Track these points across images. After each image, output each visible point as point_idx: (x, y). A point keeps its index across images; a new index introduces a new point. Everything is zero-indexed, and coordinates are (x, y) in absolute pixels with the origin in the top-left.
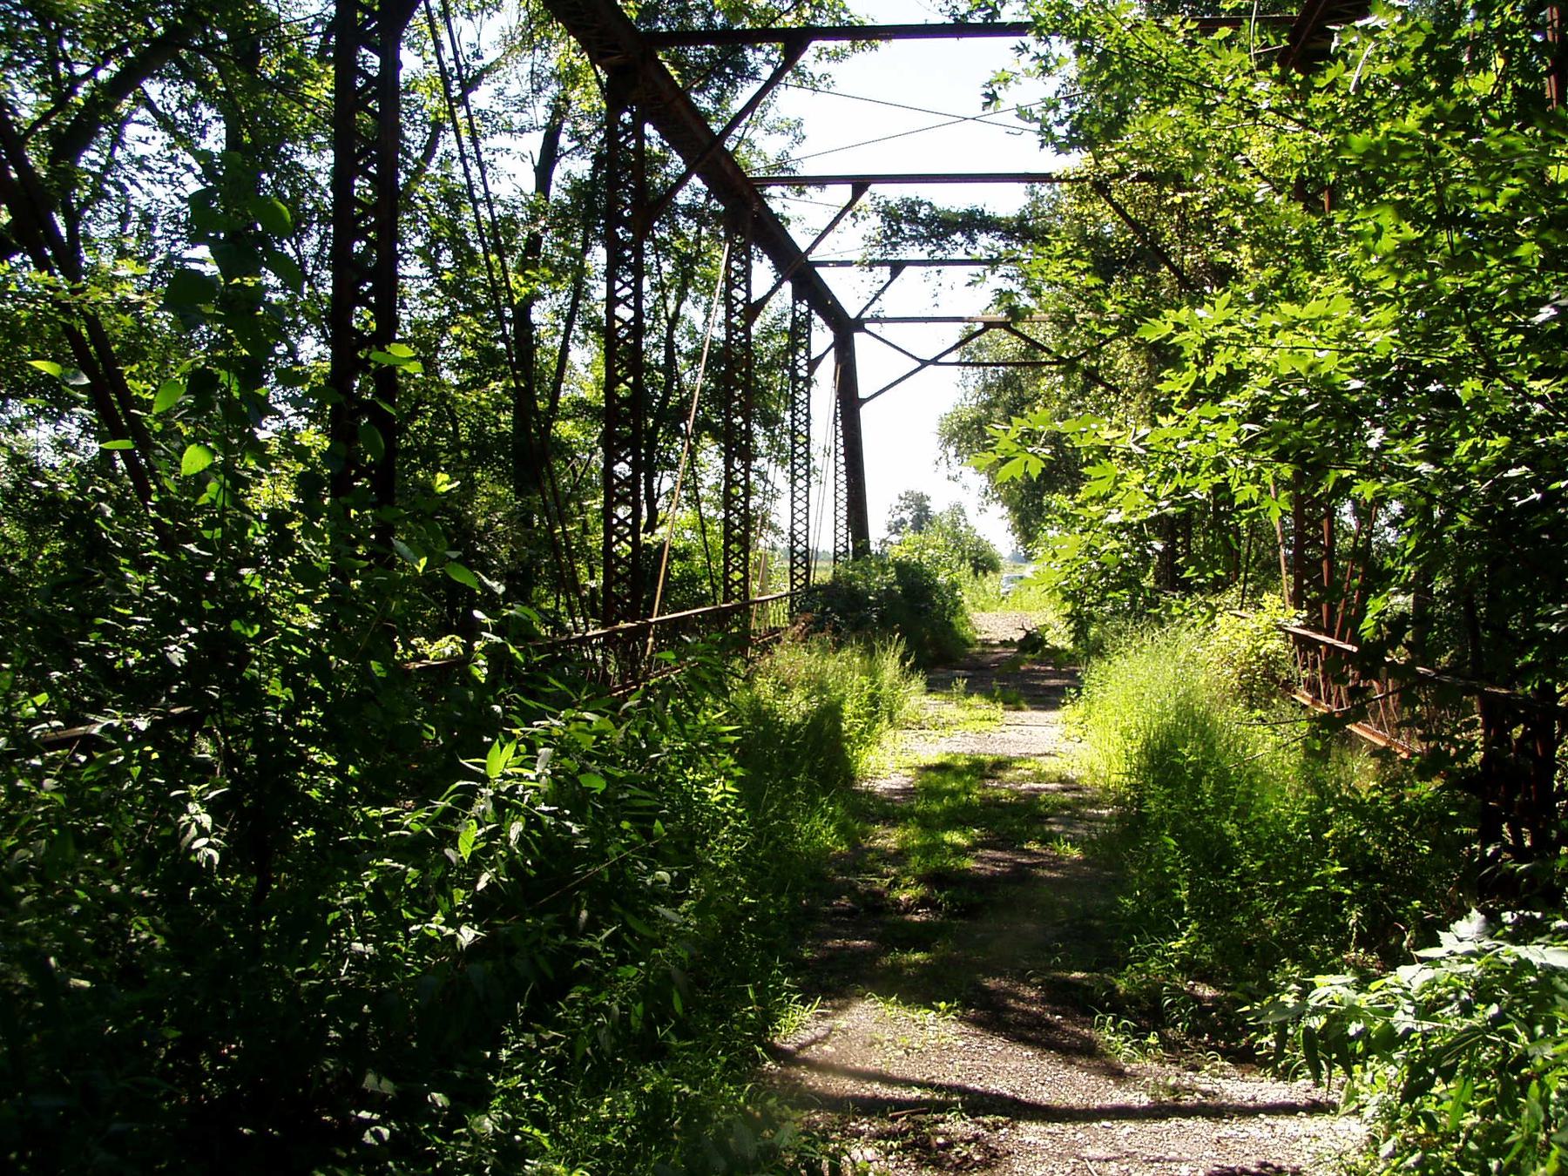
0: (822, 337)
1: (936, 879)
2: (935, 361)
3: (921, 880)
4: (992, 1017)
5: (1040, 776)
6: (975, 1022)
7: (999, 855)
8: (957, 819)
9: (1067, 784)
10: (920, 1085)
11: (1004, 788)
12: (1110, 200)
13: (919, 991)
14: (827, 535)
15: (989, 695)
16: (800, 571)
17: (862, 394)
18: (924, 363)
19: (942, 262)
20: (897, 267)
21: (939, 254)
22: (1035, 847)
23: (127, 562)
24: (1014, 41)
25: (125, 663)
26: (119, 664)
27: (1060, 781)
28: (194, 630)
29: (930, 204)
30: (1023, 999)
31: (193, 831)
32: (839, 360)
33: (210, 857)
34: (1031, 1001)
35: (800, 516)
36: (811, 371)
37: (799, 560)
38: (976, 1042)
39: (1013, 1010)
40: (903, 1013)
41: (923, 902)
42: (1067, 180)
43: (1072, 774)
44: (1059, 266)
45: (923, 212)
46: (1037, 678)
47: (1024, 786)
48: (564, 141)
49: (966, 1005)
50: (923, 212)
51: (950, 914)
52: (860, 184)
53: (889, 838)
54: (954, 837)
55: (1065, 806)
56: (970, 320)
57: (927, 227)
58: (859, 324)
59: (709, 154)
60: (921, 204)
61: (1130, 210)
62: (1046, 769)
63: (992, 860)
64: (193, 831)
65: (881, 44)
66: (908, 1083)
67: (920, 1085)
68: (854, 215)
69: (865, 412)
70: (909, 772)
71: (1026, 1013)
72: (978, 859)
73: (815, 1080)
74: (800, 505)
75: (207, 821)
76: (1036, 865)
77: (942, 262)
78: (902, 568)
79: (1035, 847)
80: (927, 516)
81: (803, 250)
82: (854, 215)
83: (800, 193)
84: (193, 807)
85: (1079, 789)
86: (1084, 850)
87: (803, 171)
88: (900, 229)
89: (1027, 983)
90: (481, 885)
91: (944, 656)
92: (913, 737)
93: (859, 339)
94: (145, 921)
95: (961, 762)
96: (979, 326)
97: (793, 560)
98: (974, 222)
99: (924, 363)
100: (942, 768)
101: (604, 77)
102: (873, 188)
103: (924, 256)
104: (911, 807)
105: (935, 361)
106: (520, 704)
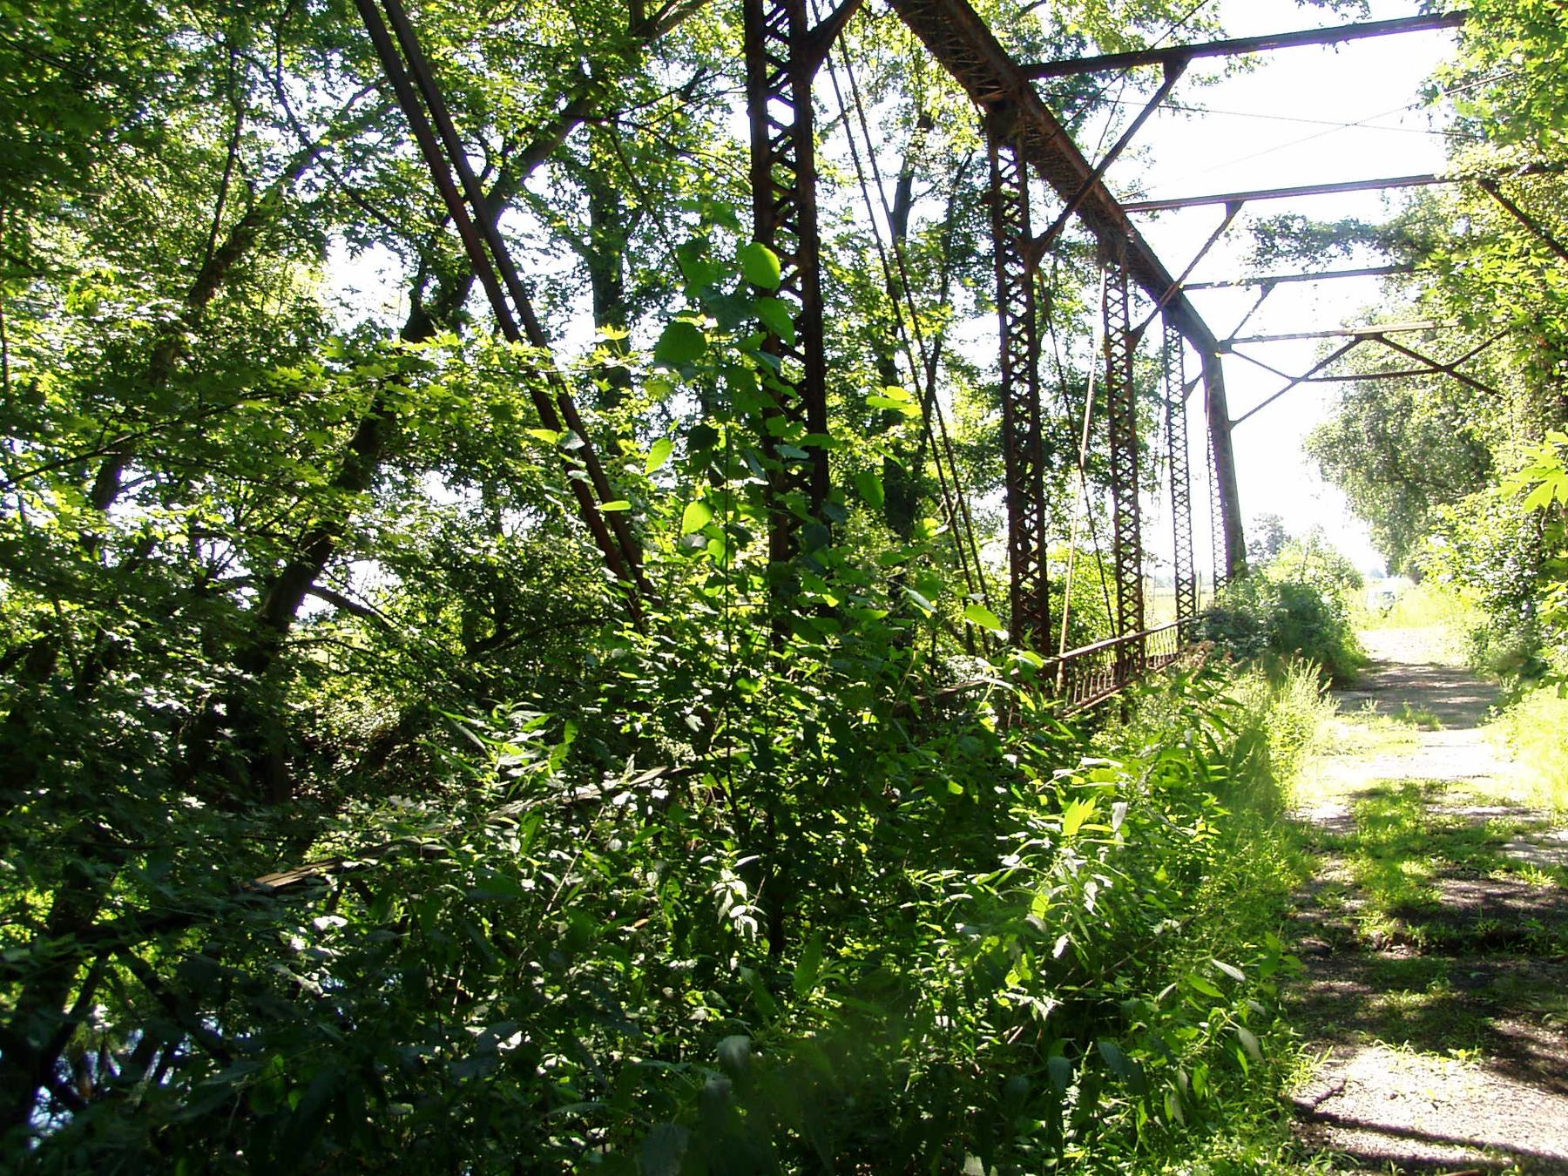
0: (1192, 363)
1: (1406, 912)
2: (1306, 378)
3: (1391, 915)
4: (1515, 1062)
5: (1481, 800)
6: (1500, 1070)
7: (1464, 885)
8: (1409, 847)
9: (1510, 807)
10: (1462, 1144)
11: (1450, 810)
12: (1499, 196)
13: (1431, 1034)
14: (1209, 560)
15: (1397, 713)
16: (1186, 598)
17: (1232, 416)
18: (1295, 381)
19: (1318, 276)
20: (1268, 285)
21: (1313, 269)
22: (1500, 875)
23: (631, 625)
24: (1452, 31)
25: (633, 728)
26: (626, 729)
27: (1504, 804)
28: (707, 692)
29: (1303, 218)
30: (1545, 1045)
31: (729, 900)
32: (1207, 385)
33: (748, 926)
34: (1555, 1047)
35: (1182, 543)
36: (1184, 398)
37: (1185, 587)
38: (1508, 1093)
39: (1537, 1058)
40: (1417, 1060)
41: (1398, 939)
42: (1451, 180)
43: (1513, 796)
44: (1512, 266)
45: (1296, 226)
46: (1443, 696)
47: (1466, 811)
48: (917, 187)
49: (1487, 1052)
50: (1296, 226)
51: (1426, 950)
52: (1233, 203)
53: (1341, 870)
54: (1409, 867)
55: (1518, 832)
56: (1326, 335)
57: (1302, 240)
58: (1226, 346)
59: (1082, 188)
60: (1293, 218)
61: (1520, 205)
62: (1485, 792)
63: (1460, 891)
64: (729, 900)
65: (1341, 44)
66: (1448, 1142)
67: (1462, 1144)
68: (1227, 235)
69: (1236, 434)
70: (1340, 800)
71: (1553, 1060)
72: (1446, 890)
73: (1343, 1138)
74: (1182, 532)
75: (741, 888)
76: (1505, 896)
77: (1318, 276)
78: (1286, 590)
79: (1500, 875)
80: (1282, 536)
81: (1176, 279)
82: (1227, 235)
83: (1154, 217)
84: (726, 874)
85: (1525, 813)
86: (1558, 879)
87: (1153, 197)
88: (1273, 246)
89: (1544, 1026)
90: (1057, 952)
91: (1348, 680)
92: (1331, 761)
93: (1227, 361)
94: (699, 995)
95: (1396, 787)
96: (1340, 342)
97: (1178, 587)
98: (1346, 234)
99: (1295, 381)
100: (1373, 794)
101: (984, 113)
102: (1248, 206)
103: (1298, 271)
104: (1355, 837)
105: (1306, 378)
106: (1031, 753)
